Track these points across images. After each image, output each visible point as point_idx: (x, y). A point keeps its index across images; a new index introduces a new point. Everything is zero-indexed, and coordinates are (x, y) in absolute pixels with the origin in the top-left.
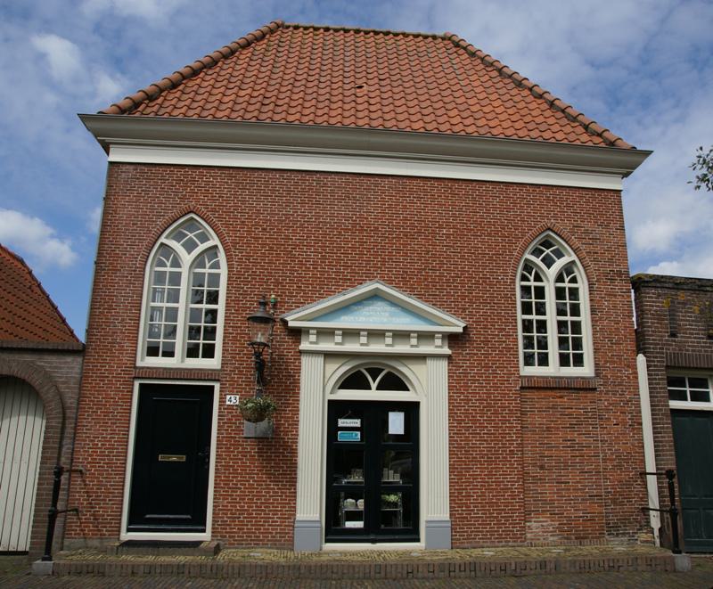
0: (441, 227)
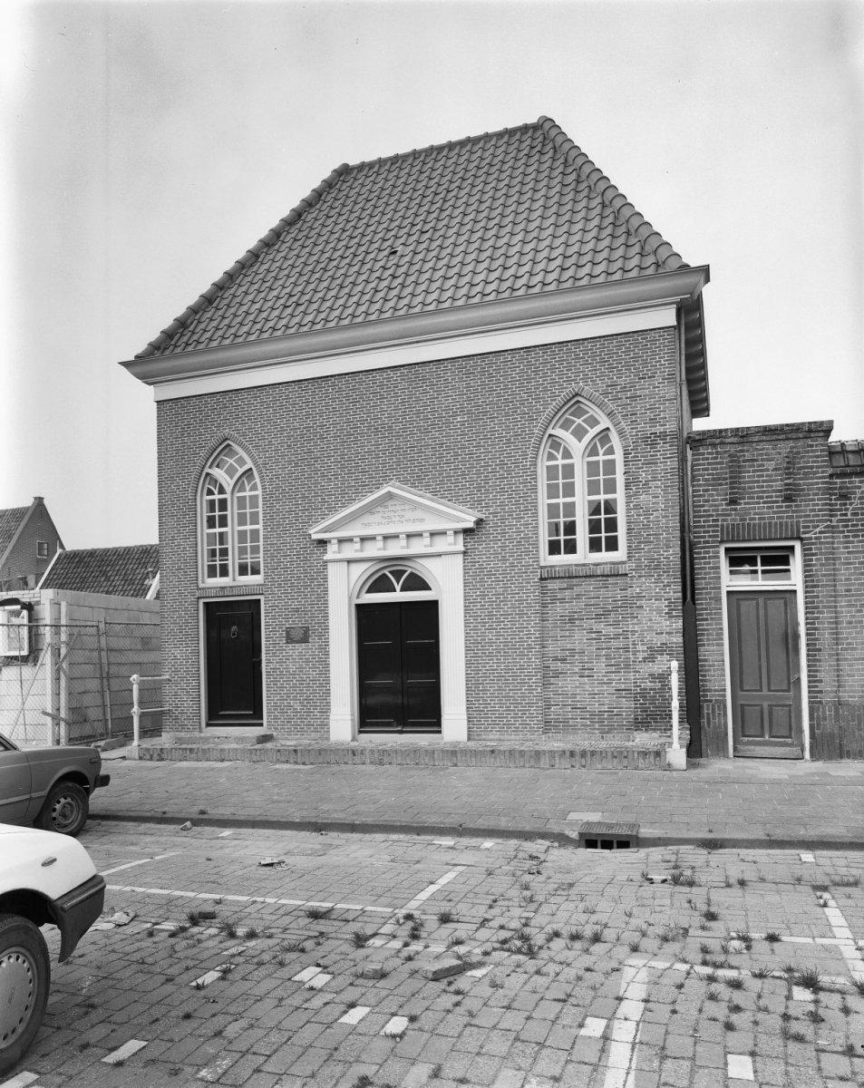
0: (455, 415)
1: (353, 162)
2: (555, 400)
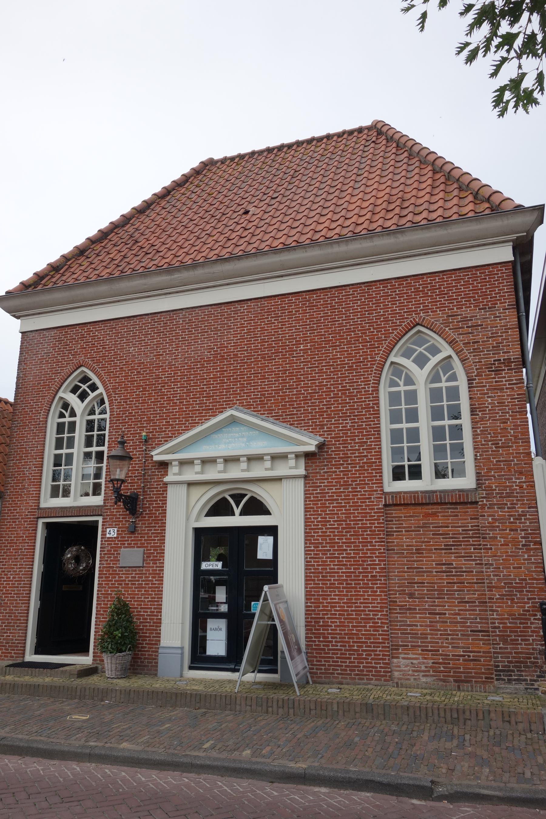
0: (298, 343)
1: (217, 156)
2: (397, 329)
